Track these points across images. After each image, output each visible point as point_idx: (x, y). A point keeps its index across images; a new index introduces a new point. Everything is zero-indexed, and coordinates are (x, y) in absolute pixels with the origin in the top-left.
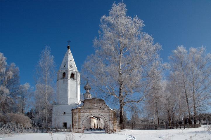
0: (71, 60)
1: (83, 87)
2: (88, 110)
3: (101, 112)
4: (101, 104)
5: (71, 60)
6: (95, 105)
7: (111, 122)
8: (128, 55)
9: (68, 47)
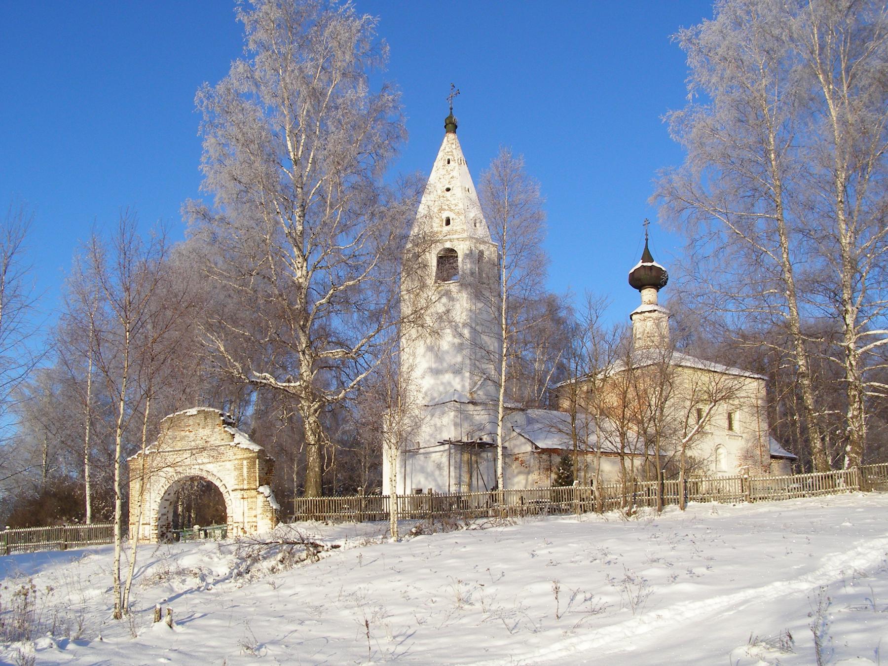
4: (207, 431)
9: (451, 126)
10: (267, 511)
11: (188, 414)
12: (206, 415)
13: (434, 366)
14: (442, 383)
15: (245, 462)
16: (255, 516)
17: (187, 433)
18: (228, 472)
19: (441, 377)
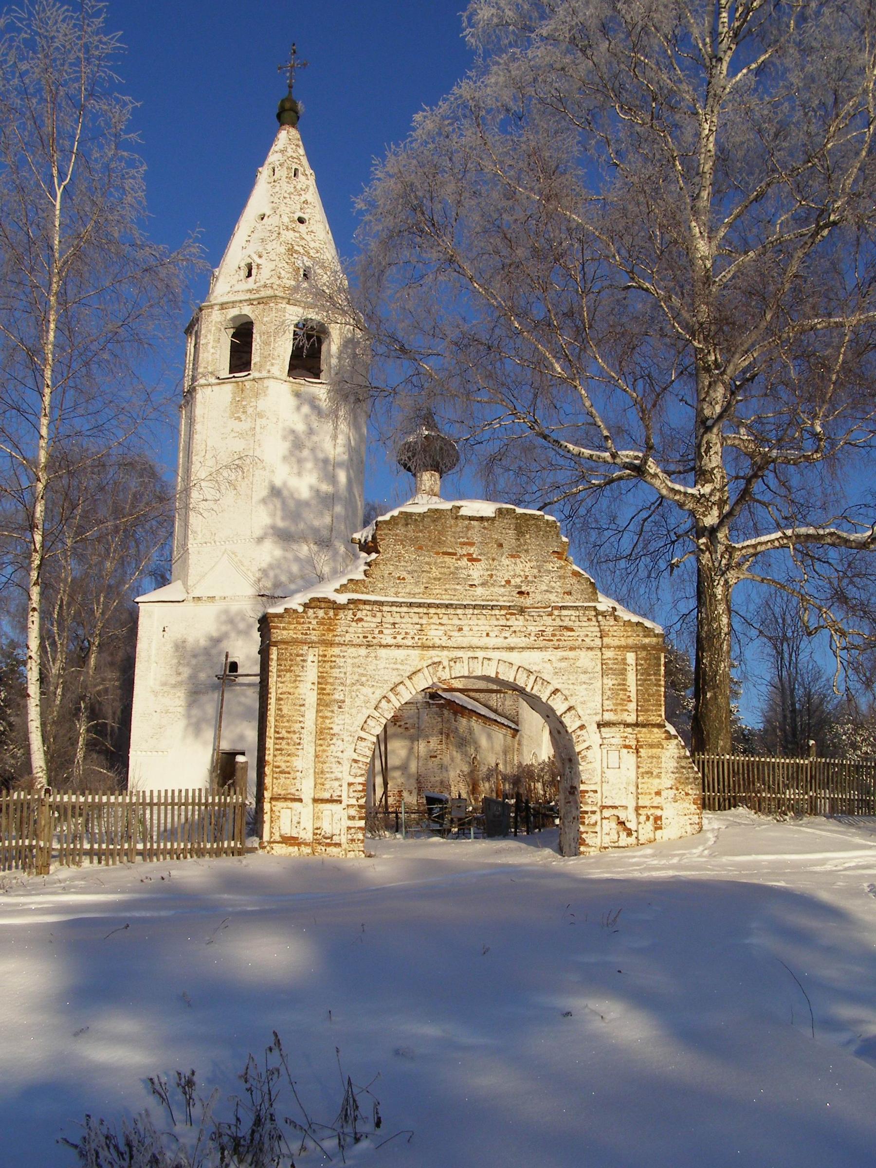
0: (301, 221)
1: (395, 466)
2: (408, 622)
3: (521, 641)
4: (523, 567)
5: (301, 221)
6: (477, 572)
7: (615, 735)
8: (581, 844)
9: (287, 115)
10: (686, 782)
11: (463, 512)
12: (523, 525)
13: (280, 524)
14: (297, 559)
15: (631, 657)
16: (658, 793)
17: (464, 562)
18: (583, 678)
19: (295, 547)
